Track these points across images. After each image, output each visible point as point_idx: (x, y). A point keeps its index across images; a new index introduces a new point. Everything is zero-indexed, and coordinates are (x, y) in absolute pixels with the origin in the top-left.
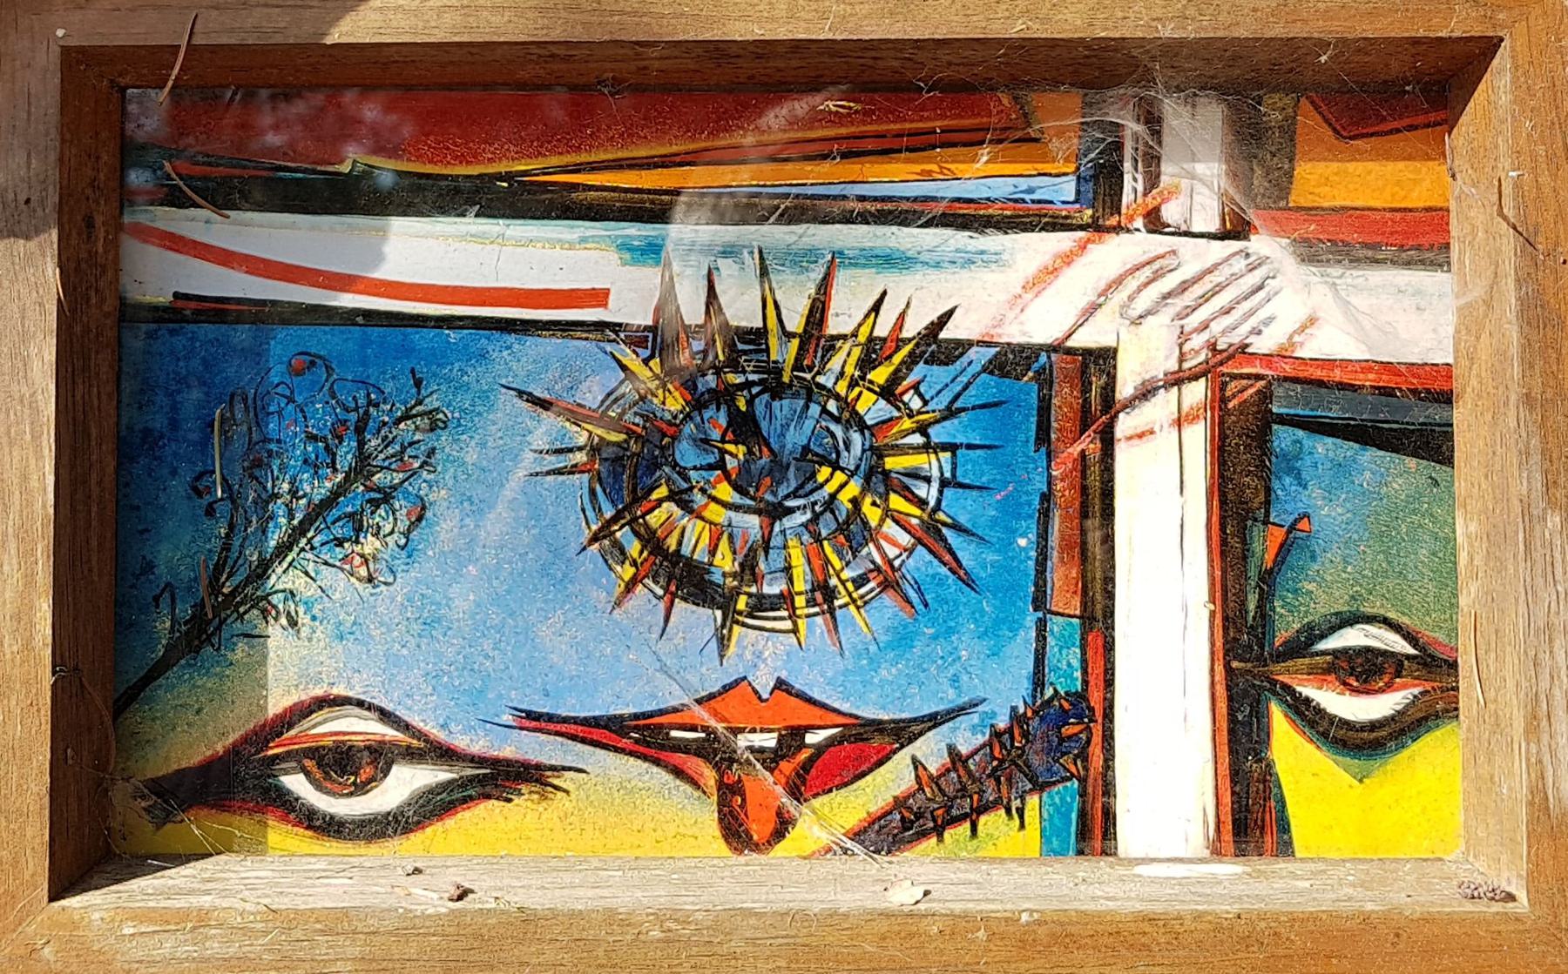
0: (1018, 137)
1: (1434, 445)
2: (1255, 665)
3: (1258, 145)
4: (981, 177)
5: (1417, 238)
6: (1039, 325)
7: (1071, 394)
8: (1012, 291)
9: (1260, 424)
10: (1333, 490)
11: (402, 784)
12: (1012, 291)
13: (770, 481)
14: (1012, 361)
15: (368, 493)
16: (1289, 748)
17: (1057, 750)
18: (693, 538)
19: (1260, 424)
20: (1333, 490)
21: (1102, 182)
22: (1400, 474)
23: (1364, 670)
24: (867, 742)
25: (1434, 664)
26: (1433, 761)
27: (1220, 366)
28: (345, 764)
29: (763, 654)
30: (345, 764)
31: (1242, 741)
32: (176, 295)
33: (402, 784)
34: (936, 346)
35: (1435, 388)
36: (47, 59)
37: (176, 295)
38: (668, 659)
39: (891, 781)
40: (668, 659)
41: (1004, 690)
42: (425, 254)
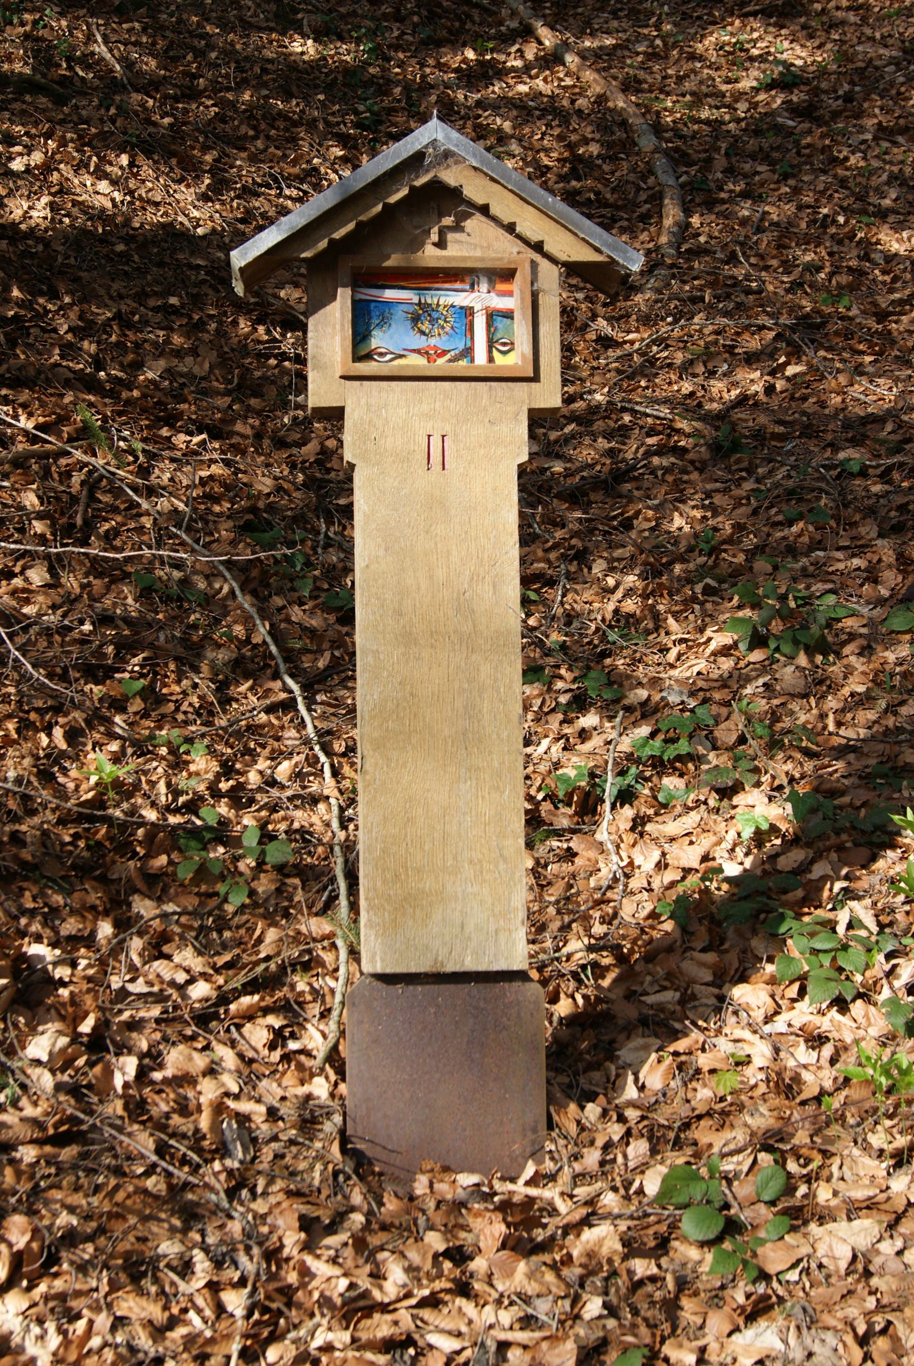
0: (463, 281)
1: (512, 318)
2: (491, 344)
3: (491, 282)
4: (458, 286)
5: (510, 294)
6: (465, 304)
7: (468, 312)
8: (461, 299)
9: (492, 316)
10: (500, 323)
11: (389, 357)
12: (461, 299)
13: (433, 321)
14: (462, 308)
15: (384, 321)
16: (495, 354)
17: (468, 352)
18: (423, 328)
19: (492, 316)
20: (500, 323)
21: (472, 286)
22: (508, 321)
23: (504, 344)
24: (444, 353)
25: (512, 344)
26: (512, 354)
27: (487, 308)
28: (382, 355)
29: (433, 341)
30: (382, 355)
31: (490, 351)
32: (352, 466)
33: (389, 357)
34: (453, 306)
35: (512, 311)
36: (169, 1065)
37: (352, 466)
38: (420, 342)
39: (448, 357)
40: (420, 342)
41: (461, 347)
42: (390, 294)
